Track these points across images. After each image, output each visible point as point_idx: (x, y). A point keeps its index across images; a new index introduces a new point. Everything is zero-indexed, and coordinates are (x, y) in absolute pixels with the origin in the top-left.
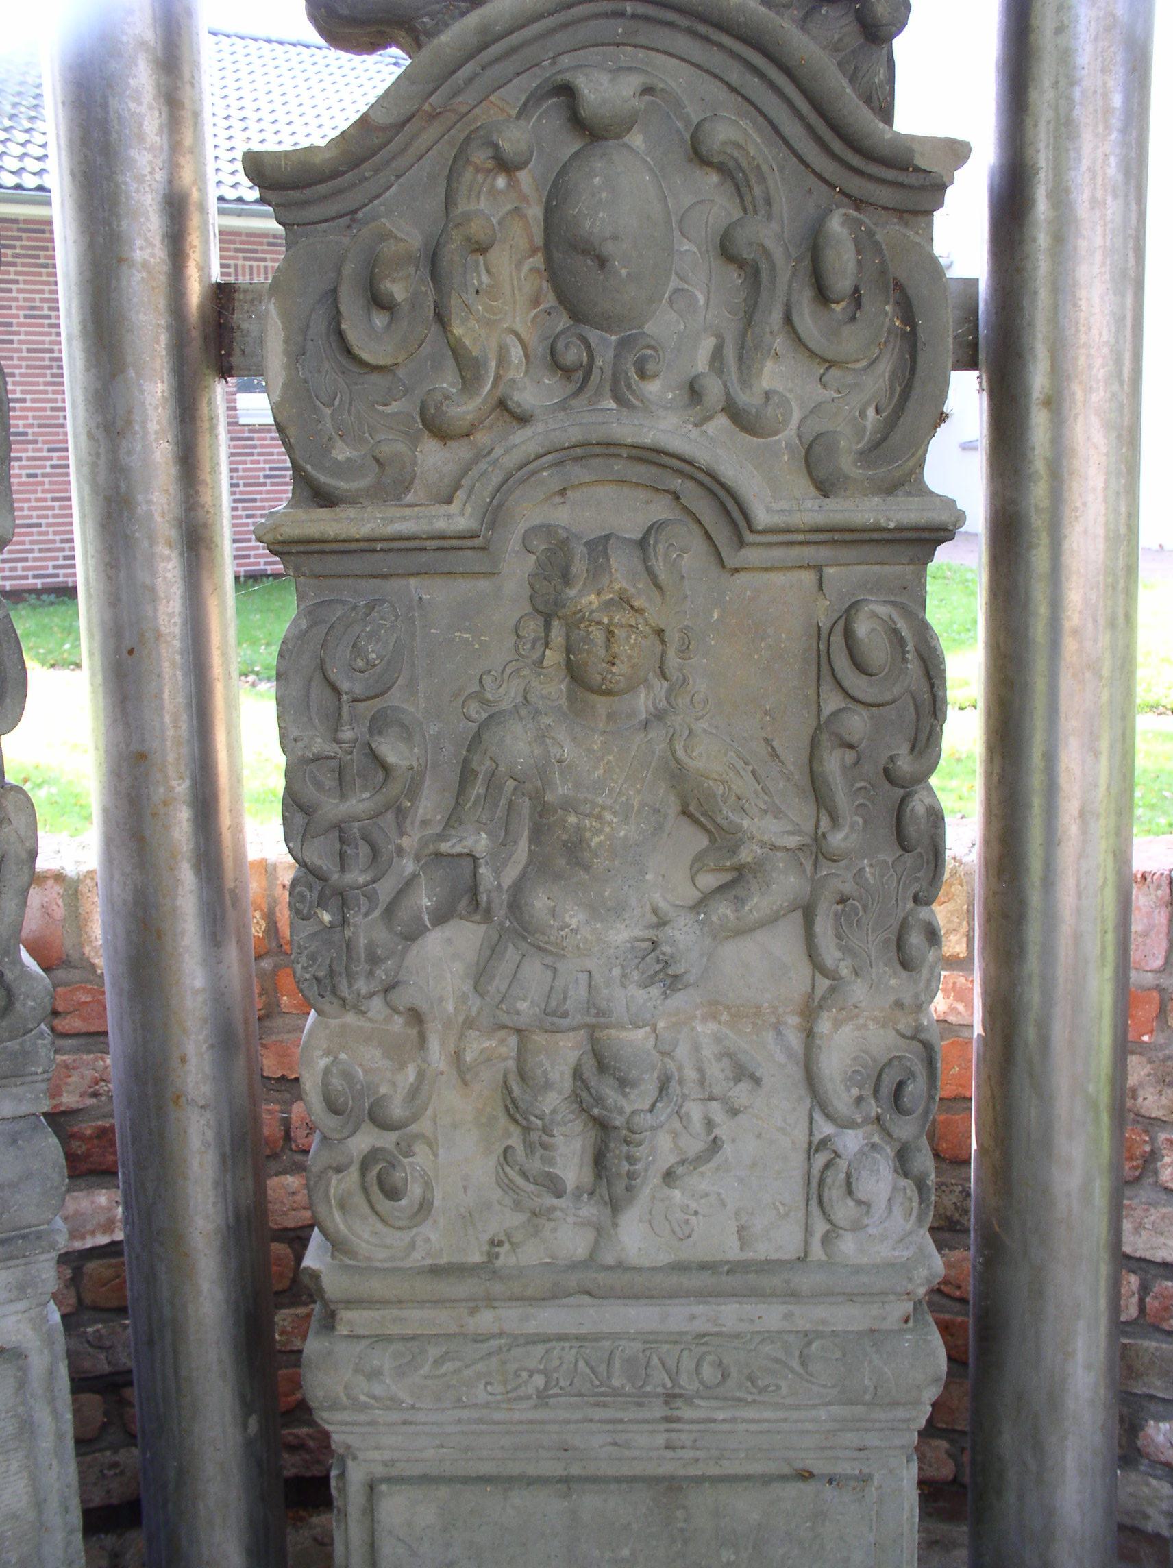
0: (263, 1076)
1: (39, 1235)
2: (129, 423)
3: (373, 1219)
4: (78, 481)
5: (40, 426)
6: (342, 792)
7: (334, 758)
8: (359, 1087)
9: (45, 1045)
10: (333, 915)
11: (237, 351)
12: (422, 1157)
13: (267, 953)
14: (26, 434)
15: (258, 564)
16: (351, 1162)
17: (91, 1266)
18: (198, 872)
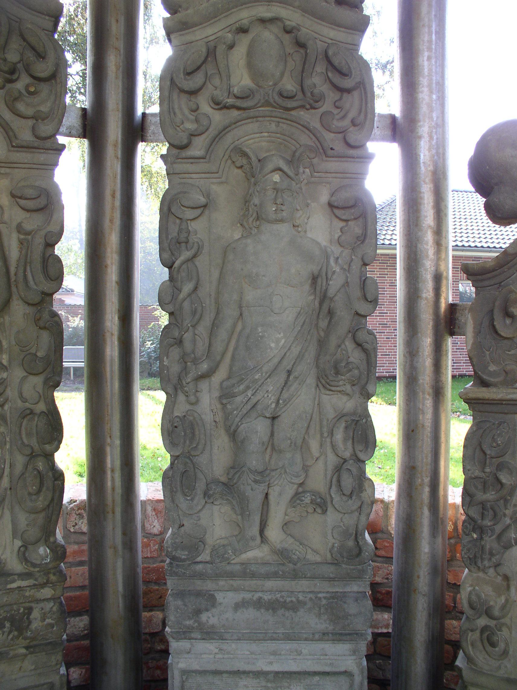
0: (447, 582)
1: (362, 635)
2: (418, 352)
3: (484, 652)
4: (399, 370)
5: (391, 322)
6: (484, 491)
7: (482, 478)
8: (482, 601)
9: (370, 569)
10: (477, 535)
11: (457, 327)
12: (505, 632)
13: (453, 537)
14: (387, 324)
15: (463, 371)
16: (477, 629)
17: (380, 639)
18: (430, 510)
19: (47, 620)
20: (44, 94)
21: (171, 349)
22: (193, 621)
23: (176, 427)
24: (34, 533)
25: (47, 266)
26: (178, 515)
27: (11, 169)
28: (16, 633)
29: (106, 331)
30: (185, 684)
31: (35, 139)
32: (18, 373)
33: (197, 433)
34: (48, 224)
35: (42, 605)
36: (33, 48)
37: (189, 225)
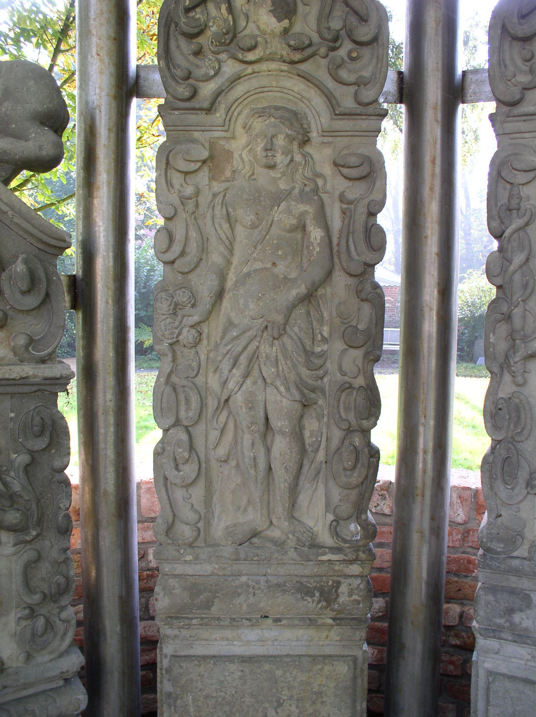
19: (354, 596)
20: (365, 60)
21: (498, 325)
22: (504, 619)
23: (500, 409)
24: (346, 509)
25: (369, 237)
26: (496, 504)
27: (333, 138)
28: (324, 604)
29: (425, 306)
30: (492, 685)
31: (357, 106)
32: (339, 345)
33: (523, 417)
34: (371, 193)
35: (350, 580)
36: (356, 13)
37: (521, 190)
